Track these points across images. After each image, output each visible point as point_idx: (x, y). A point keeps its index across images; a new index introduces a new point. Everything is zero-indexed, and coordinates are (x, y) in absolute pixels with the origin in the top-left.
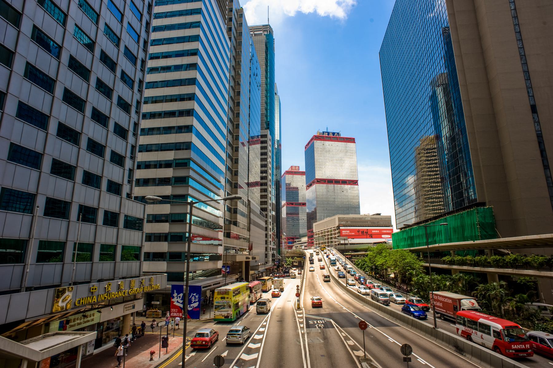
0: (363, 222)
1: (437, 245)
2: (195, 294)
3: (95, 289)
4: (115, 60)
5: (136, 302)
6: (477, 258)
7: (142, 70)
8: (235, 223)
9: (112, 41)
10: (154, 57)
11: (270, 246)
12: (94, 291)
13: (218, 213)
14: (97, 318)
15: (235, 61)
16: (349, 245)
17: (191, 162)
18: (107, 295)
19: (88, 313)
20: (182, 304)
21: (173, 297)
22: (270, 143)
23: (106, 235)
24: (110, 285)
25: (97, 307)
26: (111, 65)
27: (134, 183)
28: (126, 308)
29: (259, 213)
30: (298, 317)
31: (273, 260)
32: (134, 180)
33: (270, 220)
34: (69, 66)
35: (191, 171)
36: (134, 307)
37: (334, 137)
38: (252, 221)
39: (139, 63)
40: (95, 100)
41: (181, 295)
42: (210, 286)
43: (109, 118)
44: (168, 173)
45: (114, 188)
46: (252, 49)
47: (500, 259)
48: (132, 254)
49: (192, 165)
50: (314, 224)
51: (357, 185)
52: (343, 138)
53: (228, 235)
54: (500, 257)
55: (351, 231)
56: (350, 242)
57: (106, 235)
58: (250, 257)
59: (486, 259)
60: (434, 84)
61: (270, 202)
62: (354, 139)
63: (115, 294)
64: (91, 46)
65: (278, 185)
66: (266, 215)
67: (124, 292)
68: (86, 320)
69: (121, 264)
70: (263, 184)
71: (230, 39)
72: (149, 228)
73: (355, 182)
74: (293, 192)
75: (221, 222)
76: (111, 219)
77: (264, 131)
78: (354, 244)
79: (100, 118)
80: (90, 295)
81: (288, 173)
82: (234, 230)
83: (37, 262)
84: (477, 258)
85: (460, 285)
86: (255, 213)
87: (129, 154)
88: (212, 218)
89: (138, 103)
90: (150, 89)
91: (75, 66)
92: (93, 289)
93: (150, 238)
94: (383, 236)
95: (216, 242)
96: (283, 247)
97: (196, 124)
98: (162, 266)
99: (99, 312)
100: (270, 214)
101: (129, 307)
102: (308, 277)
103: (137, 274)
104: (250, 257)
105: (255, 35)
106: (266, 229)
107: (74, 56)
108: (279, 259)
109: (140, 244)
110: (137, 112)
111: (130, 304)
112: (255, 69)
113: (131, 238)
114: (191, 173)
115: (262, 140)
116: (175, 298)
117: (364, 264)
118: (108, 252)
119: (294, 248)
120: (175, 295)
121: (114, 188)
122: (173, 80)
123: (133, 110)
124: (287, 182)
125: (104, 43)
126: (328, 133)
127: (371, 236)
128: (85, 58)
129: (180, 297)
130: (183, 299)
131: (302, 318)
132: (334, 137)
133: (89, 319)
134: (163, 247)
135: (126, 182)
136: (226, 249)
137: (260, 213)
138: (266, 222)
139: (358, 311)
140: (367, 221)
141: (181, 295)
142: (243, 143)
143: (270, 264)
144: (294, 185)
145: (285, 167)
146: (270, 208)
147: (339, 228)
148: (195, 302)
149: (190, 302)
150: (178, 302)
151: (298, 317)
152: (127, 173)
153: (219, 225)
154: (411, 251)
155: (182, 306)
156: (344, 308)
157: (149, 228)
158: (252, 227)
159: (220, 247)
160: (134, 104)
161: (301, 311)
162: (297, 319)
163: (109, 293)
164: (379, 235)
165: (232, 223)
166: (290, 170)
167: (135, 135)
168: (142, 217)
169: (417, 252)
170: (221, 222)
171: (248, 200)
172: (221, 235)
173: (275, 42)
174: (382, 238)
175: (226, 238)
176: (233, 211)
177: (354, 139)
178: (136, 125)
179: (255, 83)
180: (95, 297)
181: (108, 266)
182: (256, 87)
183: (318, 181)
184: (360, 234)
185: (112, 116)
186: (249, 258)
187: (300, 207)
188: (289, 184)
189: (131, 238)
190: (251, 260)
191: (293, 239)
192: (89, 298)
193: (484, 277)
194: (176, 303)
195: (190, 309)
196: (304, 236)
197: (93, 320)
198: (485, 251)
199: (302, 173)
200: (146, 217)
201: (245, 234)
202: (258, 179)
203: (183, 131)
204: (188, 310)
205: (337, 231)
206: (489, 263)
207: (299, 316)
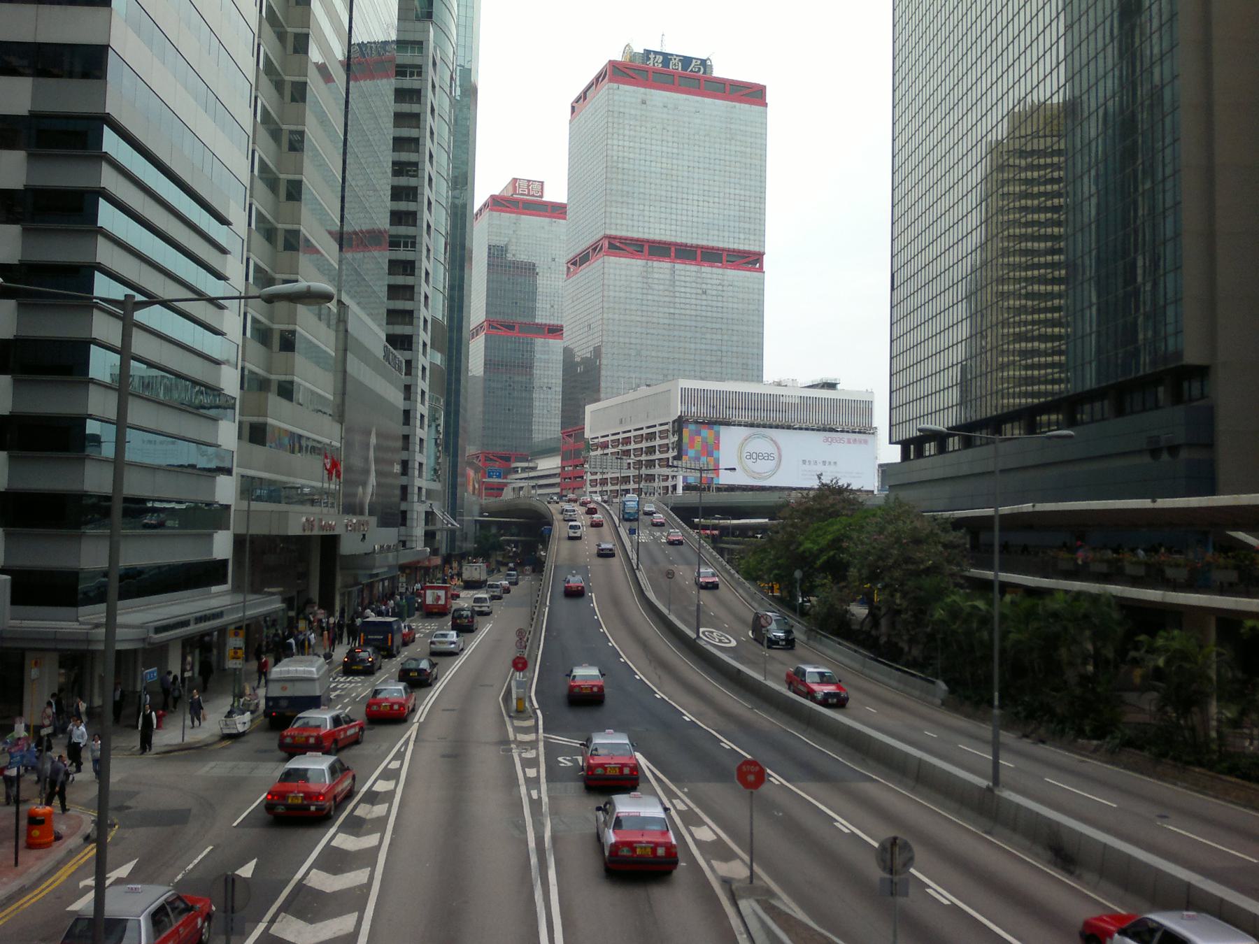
8: (286, 391)
11: (418, 482)
29: (381, 354)
31: (430, 536)
33: (423, 385)
50: (589, 409)
51: (761, 270)
53: (256, 434)
61: (423, 313)
75: (229, 381)
81: (497, 203)
88: (194, 368)
108: (452, 532)
114: (109, 180)
119: (508, 495)
131: (533, 745)
136: (249, 488)
137: (386, 357)
138: (408, 389)
144: (519, 253)
145: (488, 183)
146: (424, 337)
159: (222, 480)
161: (530, 723)
170: (229, 381)
172: (227, 433)
183: (611, 246)
187: (539, 341)
191: (507, 459)
196: (547, 452)
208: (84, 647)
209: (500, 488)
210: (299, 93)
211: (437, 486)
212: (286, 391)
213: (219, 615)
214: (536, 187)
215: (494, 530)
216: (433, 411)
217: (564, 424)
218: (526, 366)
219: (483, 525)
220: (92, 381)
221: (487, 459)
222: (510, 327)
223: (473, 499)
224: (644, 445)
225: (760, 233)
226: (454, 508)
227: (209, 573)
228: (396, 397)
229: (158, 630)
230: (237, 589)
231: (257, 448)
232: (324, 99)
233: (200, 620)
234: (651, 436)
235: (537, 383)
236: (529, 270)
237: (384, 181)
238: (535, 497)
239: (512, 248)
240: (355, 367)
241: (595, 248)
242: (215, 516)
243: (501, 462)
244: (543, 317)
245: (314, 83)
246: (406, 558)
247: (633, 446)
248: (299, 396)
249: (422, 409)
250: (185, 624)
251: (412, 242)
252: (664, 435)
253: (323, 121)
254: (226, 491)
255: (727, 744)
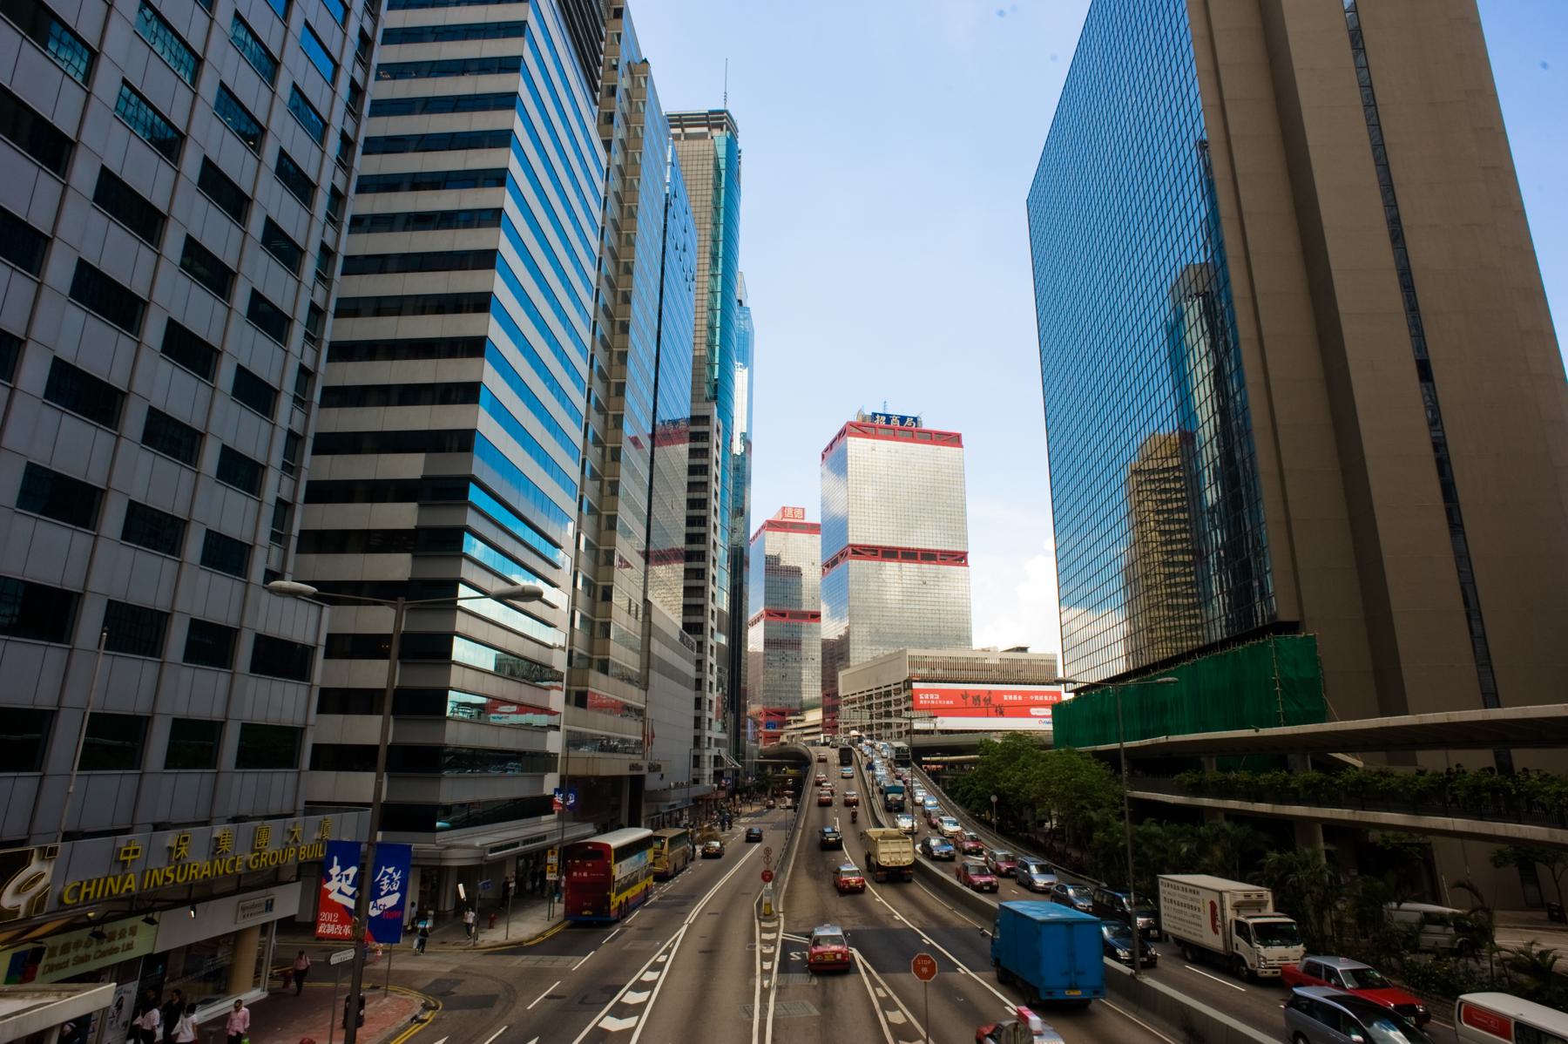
0: (977, 671)
1: (1162, 739)
2: (390, 870)
3: (136, 852)
4: (246, 188)
5: (278, 893)
6: (1264, 778)
7: (333, 219)
8: (604, 667)
9: (245, 137)
10: (368, 185)
11: (708, 734)
12: (130, 858)
13: (556, 637)
14: (143, 940)
15: (622, 208)
16: (937, 735)
17: (472, 486)
18: (174, 871)
19: (108, 928)
20: (352, 896)
21: (329, 878)
22: (716, 439)
23: (194, 691)
24: (185, 839)
25: (146, 905)
26: (234, 201)
27: (294, 543)
28: (245, 911)
29: (677, 637)
30: (763, 942)
31: (718, 775)
32: (295, 531)
33: (711, 659)
34: (96, 199)
35: (470, 513)
36: (269, 906)
37: (902, 428)
38: (654, 662)
39: (322, 201)
40: (177, 298)
41: (352, 871)
42: (516, 845)
43: (219, 353)
44: (403, 515)
45: (226, 555)
46: (674, 174)
47: (1322, 781)
48: (270, 747)
49: (475, 494)
50: (841, 674)
51: (966, 564)
52: (930, 432)
53: (579, 699)
54: (1323, 775)
55: (944, 694)
56: (940, 726)
57: (194, 691)
58: (645, 764)
59: (1287, 781)
60: (1179, 296)
61: (711, 606)
62: (958, 436)
63: (200, 866)
64: (169, 143)
65: (738, 561)
66: (700, 644)
67: (234, 862)
68: (106, 946)
69: (237, 779)
70: (694, 557)
71: (607, 145)
72: (326, 672)
73: (959, 558)
74: (782, 576)
75: (560, 662)
76: (211, 645)
77: (700, 405)
78: (952, 732)
79: (189, 350)
80: (117, 871)
81: (772, 525)
82: (601, 686)
83: (166, 767)
84: (1264, 778)
85: (1218, 853)
86: (666, 639)
87: (277, 459)
88: (530, 651)
89: (316, 312)
90: (409, 275)
91: (115, 196)
92: (127, 853)
93: (337, 701)
94: (1033, 711)
95: (542, 720)
96: (750, 737)
97: (491, 378)
98: (362, 785)
99: (151, 922)
100: (710, 642)
101: (254, 906)
102: (810, 824)
103: (287, 810)
104: (645, 764)
105: (687, 137)
106: (699, 684)
107: (114, 168)
108: (737, 772)
109: (298, 721)
110: (312, 338)
111: (258, 897)
112: (680, 232)
113: (282, 701)
114: (472, 520)
115: (697, 432)
116: (335, 879)
117: (970, 790)
118: (194, 743)
119: (783, 739)
120: (335, 870)
121: (226, 555)
122: (368, 257)
123: (297, 333)
124: (769, 552)
125: (211, 139)
126: (888, 418)
127: (1000, 712)
128: (147, 175)
129: (347, 877)
130: (357, 882)
131: (772, 943)
132: (902, 428)
133: (118, 943)
134: (367, 730)
135: (264, 536)
136: (574, 741)
137: (682, 639)
138: (699, 664)
139: (934, 925)
140: (989, 668)
141: (352, 871)
142: (635, 441)
143: (708, 783)
144: (787, 561)
145: (761, 508)
146: (712, 623)
147: (910, 687)
148: (389, 893)
149: (376, 894)
150: (340, 891)
151: (763, 942)
152: (268, 513)
153: (551, 668)
154: (1096, 754)
155: (351, 904)
156: (898, 916)
157: (326, 672)
158: (655, 677)
159: (552, 734)
160: (302, 314)
161: (775, 924)
162: (758, 947)
163: (179, 863)
164: (1022, 710)
165: (595, 664)
166: (779, 519)
167: (301, 401)
168: (309, 641)
169: (1111, 758)
170: (560, 662)
171: (646, 601)
172: (556, 700)
173: (743, 160)
174: (1029, 715)
175: (572, 709)
176: (596, 626)
177: (958, 436)
178: (306, 375)
179: (679, 272)
180: (131, 876)
181: (192, 782)
182: (681, 281)
183: (854, 552)
184: (970, 704)
185: (229, 347)
186: (640, 768)
187: (805, 623)
188: (777, 559)
189: (282, 701)
190: (645, 771)
191: (782, 714)
192: (111, 880)
193: (1283, 831)
194: (335, 896)
195: (374, 913)
196: (813, 707)
197: (129, 947)
198: (1290, 757)
199: (813, 529)
200: (323, 640)
201: (634, 696)
202: (680, 543)
203: (453, 396)
204: (370, 917)
205: (903, 695)
206: (1295, 790)
207: (766, 936)
208: (436, 863)
209: (777, 737)
210: (616, 455)
211: (723, 736)
212: (604, 667)
213: (544, 838)
214: (799, 512)
215: (769, 771)
216: (719, 680)
217: (824, 687)
218: (796, 644)
219: (762, 766)
220: (455, 663)
221: (768, 714)
222: (783, 615)
223: (756, 745)
224: (883, 700)
225: (964, 538)
226: (738, 751)
227: (541, 806)
228: (690, 670)
229: (493, 850)
230: (561, 818)
231: (580, 711)
232: (634, 462)
233: (526, 842)
234: (888, 694)
235: (804, 655)
236: (796, 572)
237: (680, 512)
238: (801, 744)
239: (783, 558)
240: (656, 647)
241: (843, 554)
242: (544, 762)
243: (778, 717)
244: (807, 607)
245: (628, 450)
246: (696, 791)
247: (875, 701)
248: (612, 670)
249: (712, 678)
250: (516, 845)
251: (702, 556)
252: (898, 692)
253: (634, 473)
254: (554, 743)
255: (927, 940)
